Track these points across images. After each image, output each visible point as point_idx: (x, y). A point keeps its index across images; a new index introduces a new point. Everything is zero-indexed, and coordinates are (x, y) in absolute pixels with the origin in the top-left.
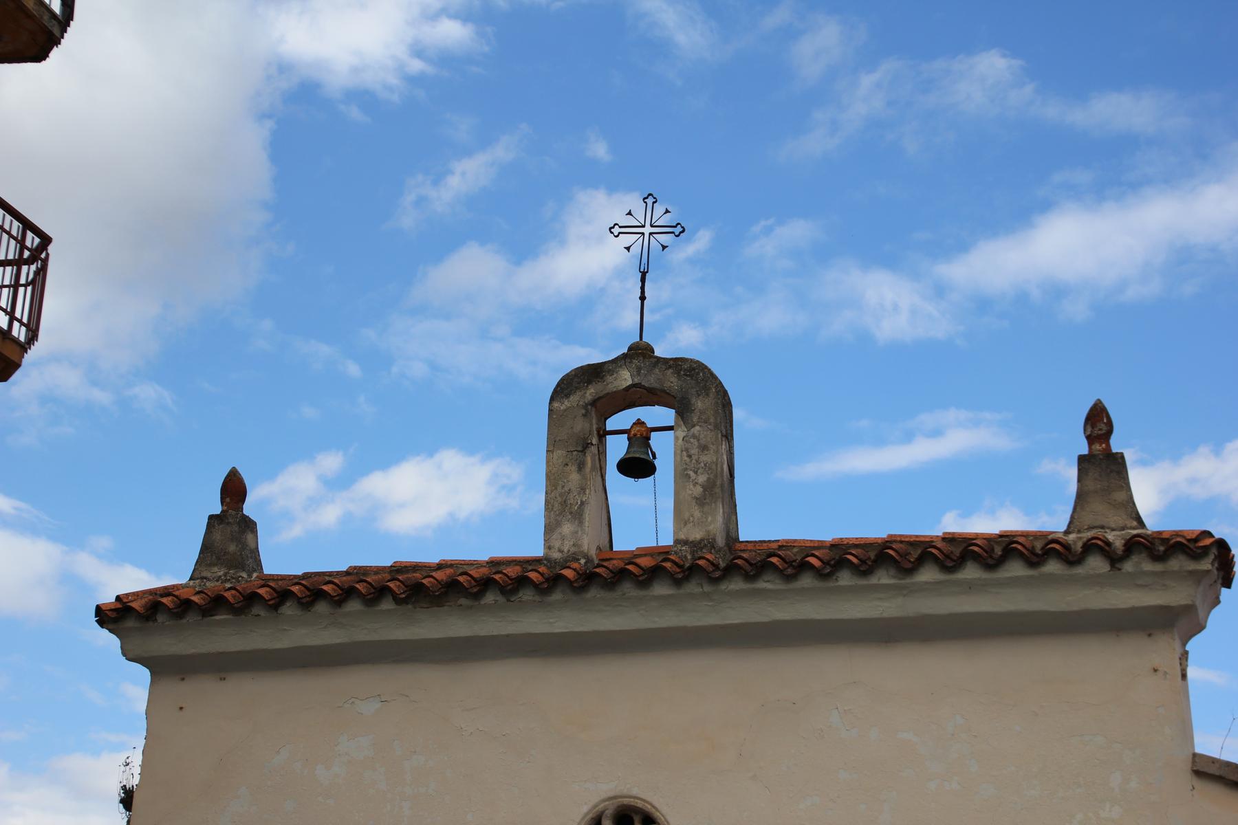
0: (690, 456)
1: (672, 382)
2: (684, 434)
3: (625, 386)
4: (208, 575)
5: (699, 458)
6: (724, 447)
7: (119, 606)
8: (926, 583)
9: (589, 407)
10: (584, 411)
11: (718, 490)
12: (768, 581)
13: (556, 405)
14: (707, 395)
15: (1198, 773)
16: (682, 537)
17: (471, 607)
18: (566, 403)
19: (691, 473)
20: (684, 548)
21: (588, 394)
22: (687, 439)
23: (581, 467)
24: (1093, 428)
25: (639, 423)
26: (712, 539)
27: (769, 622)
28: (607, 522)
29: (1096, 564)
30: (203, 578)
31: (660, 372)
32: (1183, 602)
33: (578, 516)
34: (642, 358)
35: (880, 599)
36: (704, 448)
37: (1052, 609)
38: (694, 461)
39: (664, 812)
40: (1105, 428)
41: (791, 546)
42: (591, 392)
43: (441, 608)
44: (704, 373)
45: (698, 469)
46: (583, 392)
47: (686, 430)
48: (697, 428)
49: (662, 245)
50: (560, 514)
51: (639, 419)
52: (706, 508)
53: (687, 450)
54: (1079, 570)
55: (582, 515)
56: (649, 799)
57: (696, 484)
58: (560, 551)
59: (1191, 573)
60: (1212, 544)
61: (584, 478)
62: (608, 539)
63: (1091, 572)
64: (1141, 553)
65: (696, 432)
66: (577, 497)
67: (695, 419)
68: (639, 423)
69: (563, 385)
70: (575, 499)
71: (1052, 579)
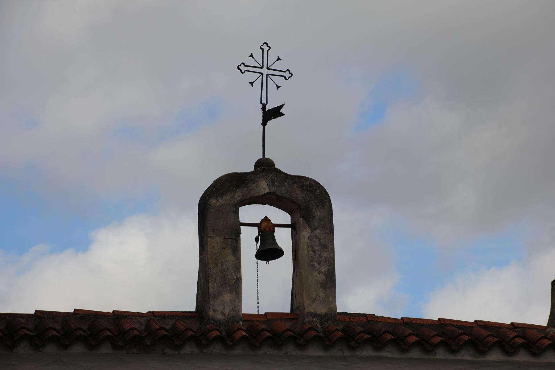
0: (314, 251)
1: (297, 194)
3: (263, 193)
5: (321, 253)
8: (493, 361)
12: (389, 352)
14: (323, 207)
19: (316, 264)
20: (314, 319)
21: (237, 196)
22: (311, 238)
25: (266, 220)
26: (333, 314)
38: (317, 255)
41: (377, 321)
45: (321, 261)
47: (310, 231)
48: (318, 231)
49: (254, 82)
51: (266, 217)
53: (312, 246)
55: (238, 288)
65: (317, 234)
66: (233, 274)
67: (316, 224)
69: (217, 187)
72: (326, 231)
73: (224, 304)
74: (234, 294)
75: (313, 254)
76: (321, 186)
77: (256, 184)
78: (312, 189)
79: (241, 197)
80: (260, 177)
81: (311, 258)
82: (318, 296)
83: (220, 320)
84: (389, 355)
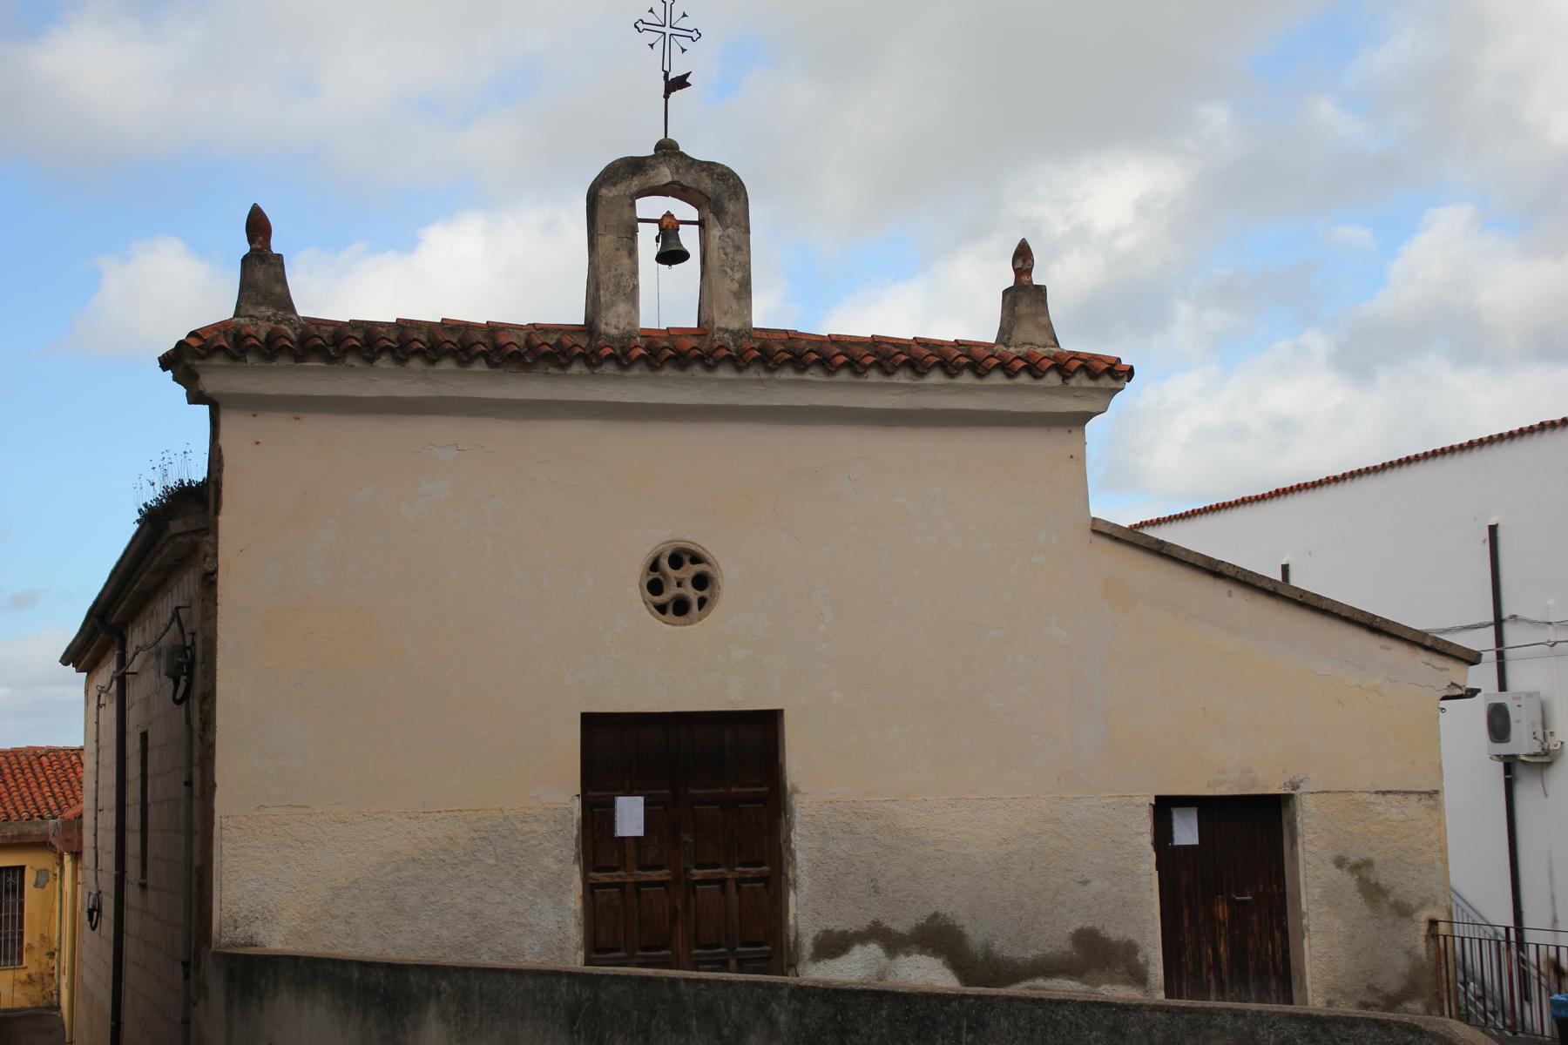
0: (726, 254)
2: (720, 234)
4: (256, 313)
8: (933, 385)
12: (812, 374)
14: (738, 199)
15: (1095, 532)
18: (613, 190)
19: (729, 270)
20: (725, 336)
21: (633, 185)
24: (1024, 263)
25: (669, 215)
27: (807, 407)
29: (1053, 379)
31: (696, 172)
34: (679, 158)
35: (895, 394)
37: (1015, 410)
39: (713, 554)
43: (528, 374)
44: (734, 179)
46: (628, 183)
48: (731, 229)
50: (615, 294)
51: (668, 212)
53: (723, 248)
54: (1041, 383)
56: (699, 544)
57: (732, 280)
58: (617, 328)
63: (1048, 385)
64: (1081, 373)
67: (729, 221)
68: (669, 215)
73: (618, 317)
74: (630, 304)
80: (661, 163)
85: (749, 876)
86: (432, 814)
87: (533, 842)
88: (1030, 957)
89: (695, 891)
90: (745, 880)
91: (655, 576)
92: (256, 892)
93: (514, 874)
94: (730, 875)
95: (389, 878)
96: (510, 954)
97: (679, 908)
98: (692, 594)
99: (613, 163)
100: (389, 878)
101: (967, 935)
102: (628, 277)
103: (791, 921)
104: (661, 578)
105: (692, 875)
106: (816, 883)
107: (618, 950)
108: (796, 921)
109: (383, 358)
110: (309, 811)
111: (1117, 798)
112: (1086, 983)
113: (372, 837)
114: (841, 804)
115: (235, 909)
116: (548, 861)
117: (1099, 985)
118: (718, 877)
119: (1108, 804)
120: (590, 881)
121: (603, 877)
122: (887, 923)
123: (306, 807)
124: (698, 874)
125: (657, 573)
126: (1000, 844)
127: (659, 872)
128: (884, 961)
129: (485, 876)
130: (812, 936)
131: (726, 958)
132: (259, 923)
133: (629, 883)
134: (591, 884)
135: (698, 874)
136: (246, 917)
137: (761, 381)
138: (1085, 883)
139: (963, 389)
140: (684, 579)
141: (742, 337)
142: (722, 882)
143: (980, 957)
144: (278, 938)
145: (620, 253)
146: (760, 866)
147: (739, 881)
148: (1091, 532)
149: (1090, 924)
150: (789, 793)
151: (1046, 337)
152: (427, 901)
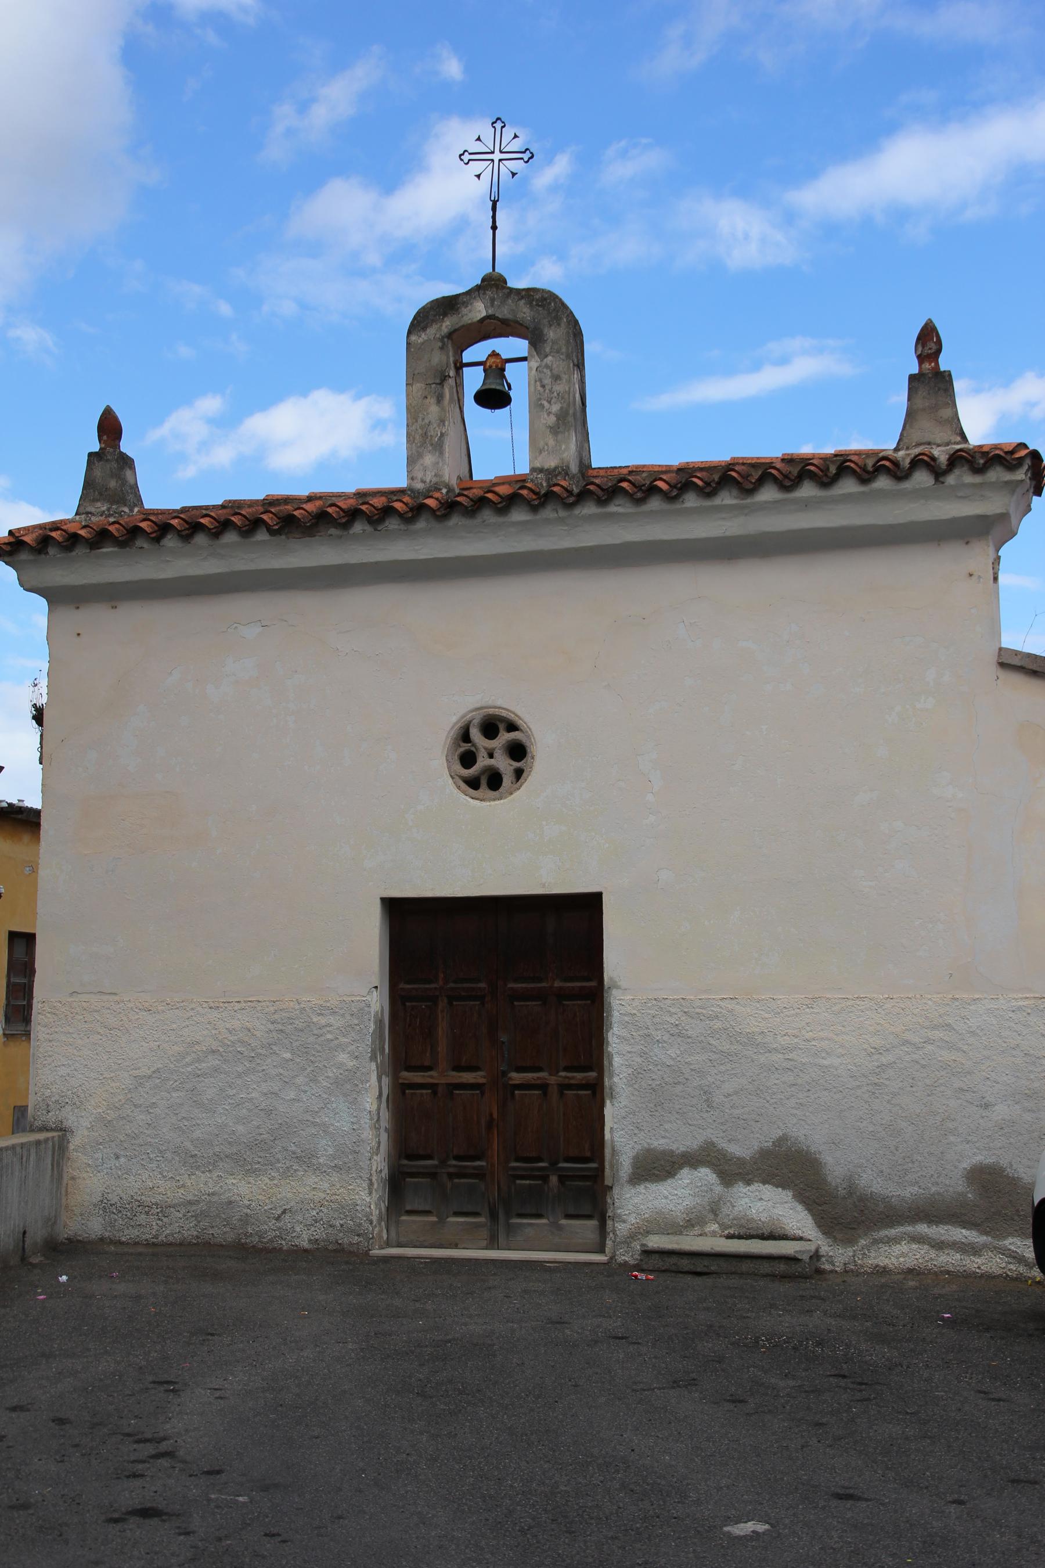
0: (543, 386)
1: (524, 313)
3: (479, 318)
6: (575, 376)
7: (12, 540)
8: (766, 502)
9: (446, 340)
10: (440, 344)
11: (570, 419)
12: (619, 505)
13: (413, 338)
14: (559, 325)
15: (1002, 665)
16: (538, 465)
17: (340, 537)
20: (539, 476)
23: (440, 399)
25: (494, 354)
28: (466, 453)
29: (922, 478)
30: (87, 513)
31: (513, 302)
32: (999, 511)
33: (438, 447)
35: (724, 519)
36: (556, 378)
38: (547, 391)
40: (934, 347)
42: (447, 324)
43: (313, 538)
44: (555, 303)
45: (552, 398)
46: (439, 324)
47: (539, 360)
48: (550, 358)
50: (421, 446)
51: (494, 351)
52: (560, 437)
53: (540, 380)
54: (907, 485)
55: (442, 446)
57: (549, 413)
59: (1007, 483)
60: (1026, 455)
61: (443, 409)
62: (467, 470)
65: (548, 362)
67: (548, 350)
68: (494, 354)
70: (435, 431)
71: (882, 494)
72: (561, 356)
74: (437, 454)
75: (541, 390)
76: (557, 297)
77: (470, 307)
78: (545, 303)
79: (449, 327)
81: (538, 396)
82: (547, 444)
83: (419, 490)
84: (620, 510)
85: (572, 1082)
86: (232, 1004)
87: (329, 1036)
88: (908, 1195)
89: (513, 1094)
90: (570, 1087)
91: (467, 748)
92: (67, 1078)
93: (309, 1069)
94: (553, 1080)
95: (189, 1069)
96: (303, 1154)
97: (495, 1116)
98: (504, 764)
99: (423, 308)
100: (189, 1069)
101: (825, 1163)
102: (435, 425)
103: (607, 1136)
104: (473, 749)
105: (510, 1079)
106: (636, 1093)
107: (429, 1157)
108: (612, 1137)
109: (169, 537)
110: (117, 998)
111: (1032, 1002)
112: (987, 1233)
113: (174, 1026)
114: (668, 1002)
115: (48, 1093)
116: (342, 1057)
117: (1005, 1238)
118: (539, 1082)
119: (1020, 1008)
120: (401, 1081)
121: (417, 1077)
122: (722, 1144)
123: (115, 994)
124: (516, 1077)
125: (470, 745)
126: (870, 1055)
127: (474, 1074)
128: (719, 1189)
129: (282, 1071)
130: (631, 1154)
131: (548, 1173)
132: (68, 1108)
133: (441, 1084)
134: (402, 1084)
135: (516, 1077)
136: (57, 1101)
137: (561, 521)
138: (987, 1106)
139: (807, 505)
140: (494, 749)
141: (556, 476)
142: (544, 1087)
143: (842, 1192)
144: (85, 1124)
145: (428, 401)
146: (587, 1072)
147: (563, 1087)
148: (998, 666)
149: (990, 1160)
150: (606, 988)
151: (949, 433)
152: (224, 1095)
